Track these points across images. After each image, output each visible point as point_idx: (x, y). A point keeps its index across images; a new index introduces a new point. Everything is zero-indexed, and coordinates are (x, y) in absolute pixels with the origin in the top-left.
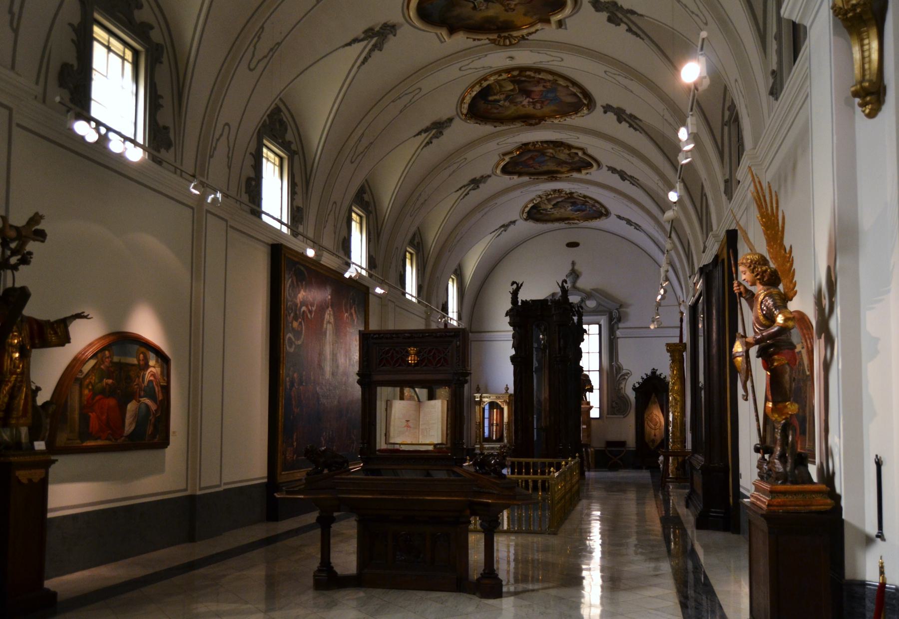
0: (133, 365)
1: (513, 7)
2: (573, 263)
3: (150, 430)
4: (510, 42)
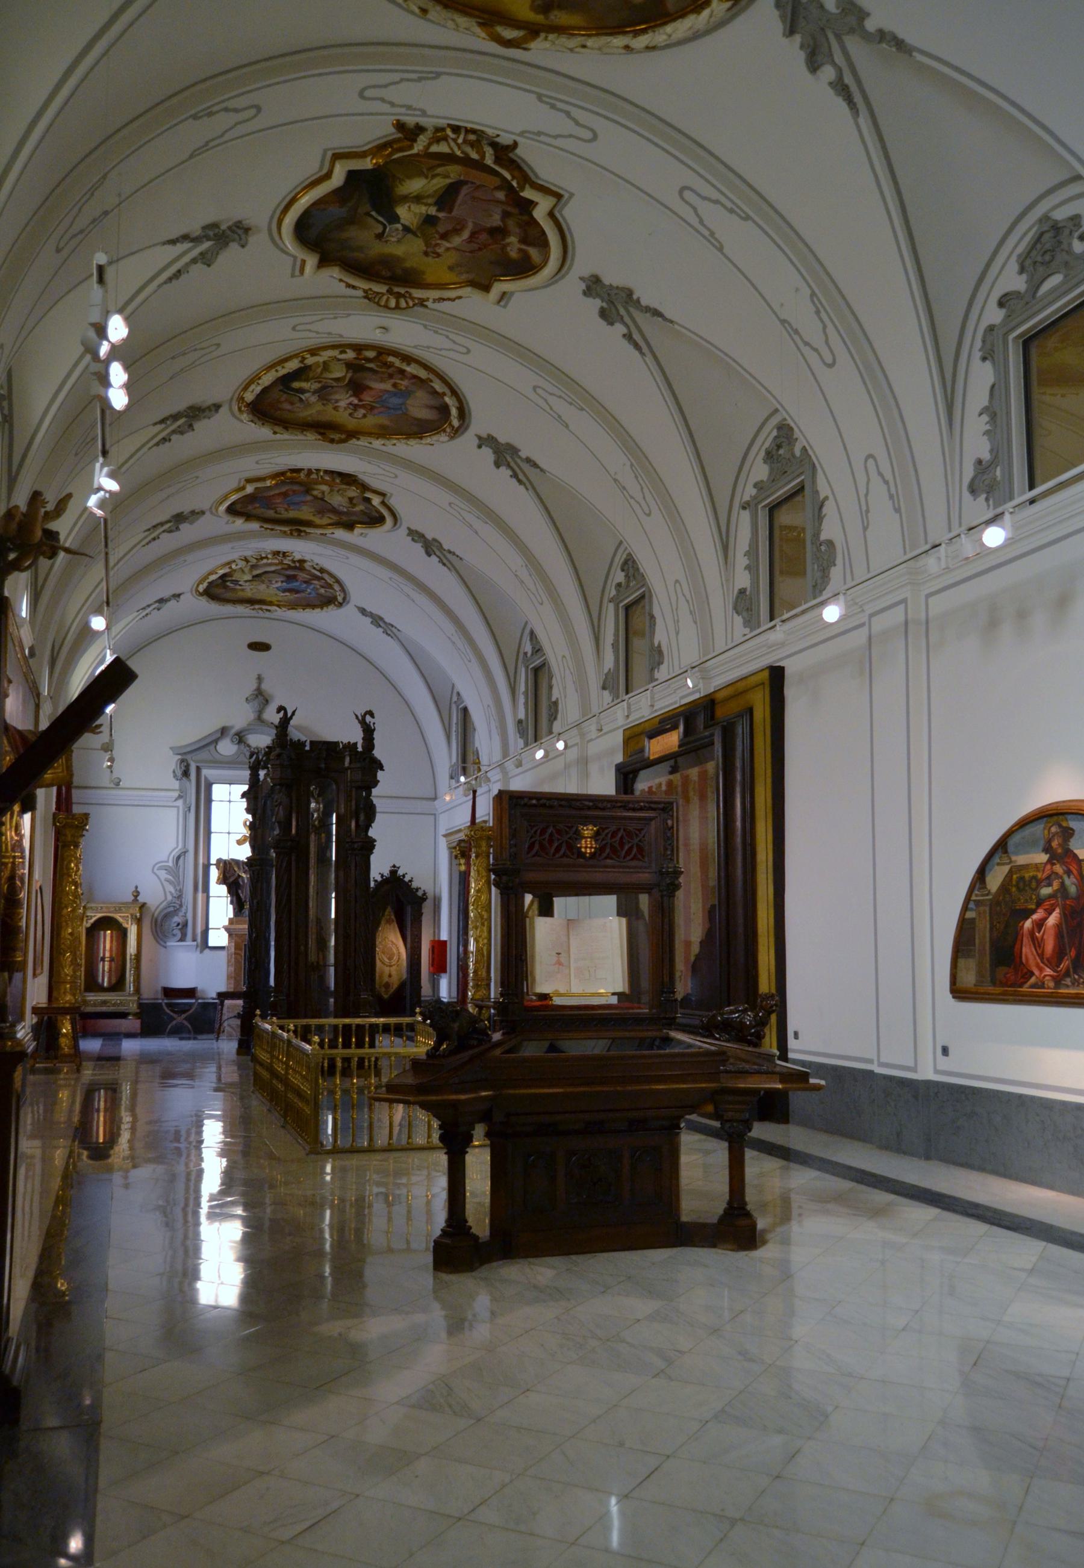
1: (440, 250)
2: (260, 679)
4: (397, 303)
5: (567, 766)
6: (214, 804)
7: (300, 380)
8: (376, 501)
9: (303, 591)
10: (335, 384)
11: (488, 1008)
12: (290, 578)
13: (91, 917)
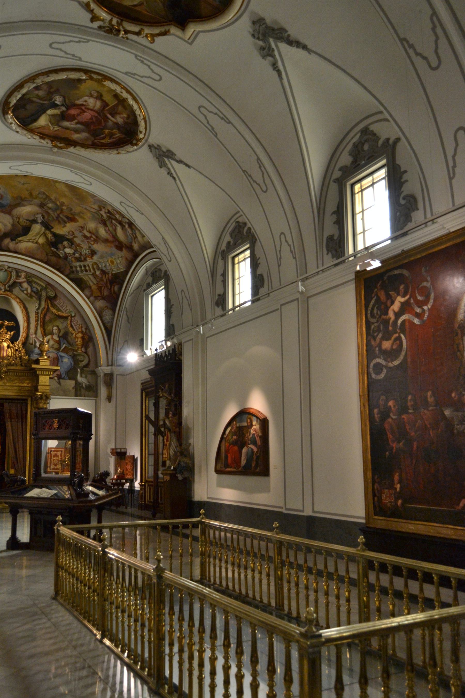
0: (245, 427)
3: (254, 464)
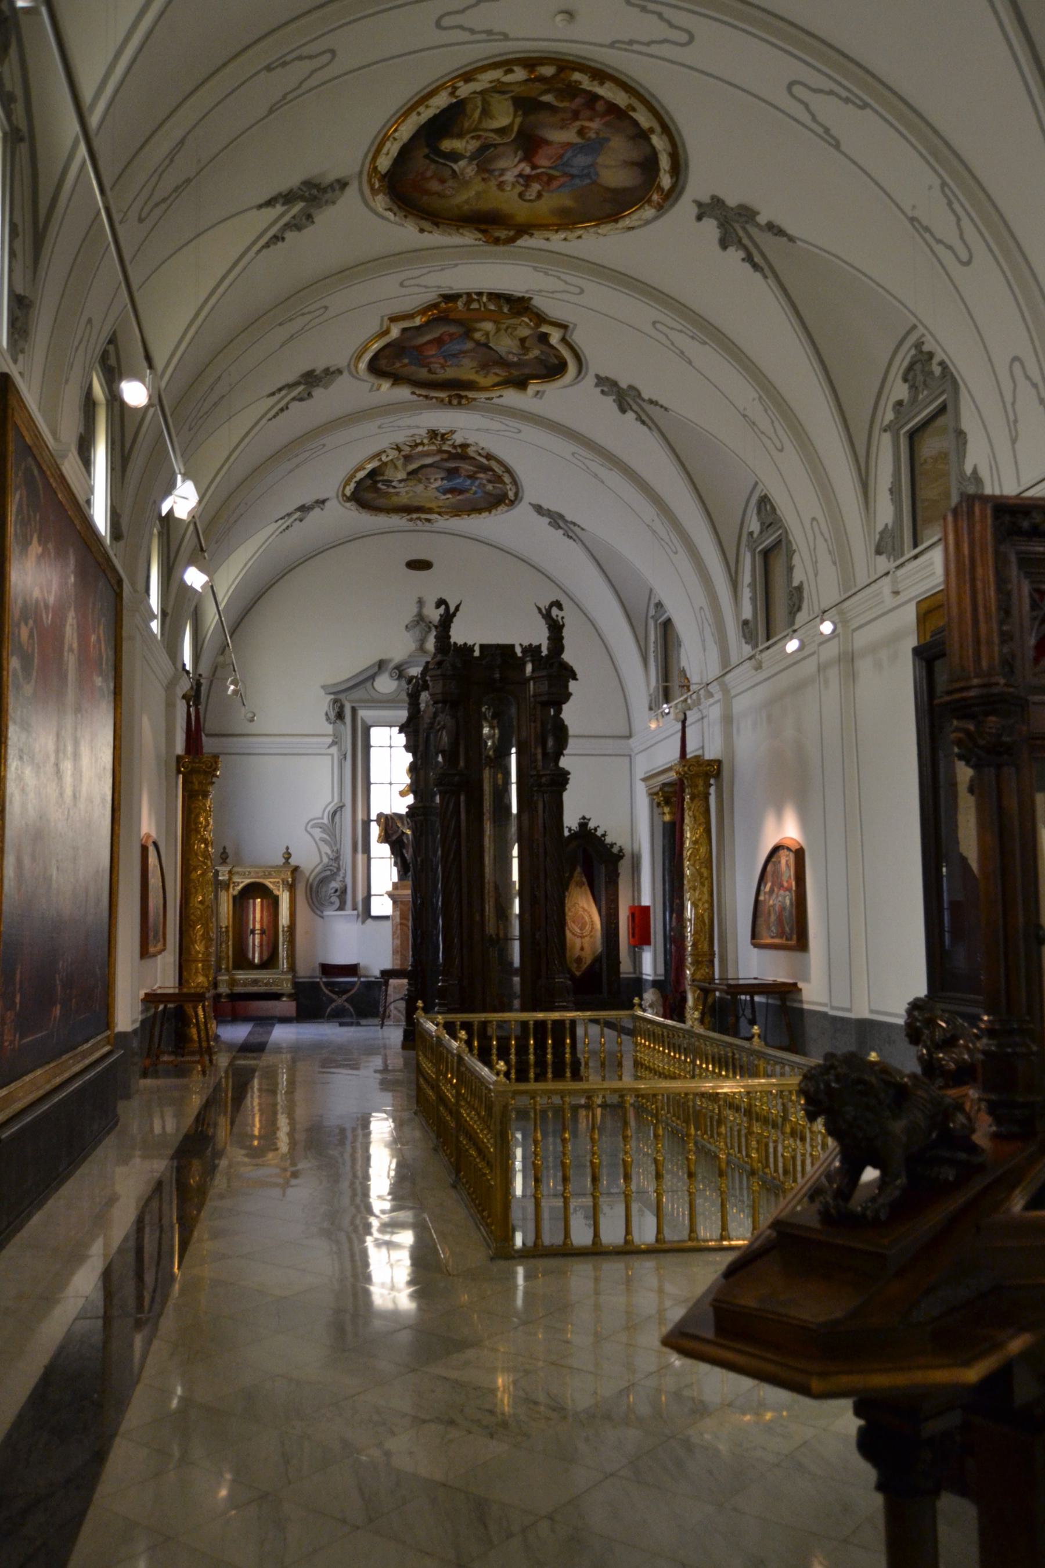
5: (821, 668)
6: (372, 750)
7: (452, 136)
8: (555, 338)
9: (467, 491)
10: (498, 140)
11: (714, 990)
12: (452, 473)
13: (238, 884)
